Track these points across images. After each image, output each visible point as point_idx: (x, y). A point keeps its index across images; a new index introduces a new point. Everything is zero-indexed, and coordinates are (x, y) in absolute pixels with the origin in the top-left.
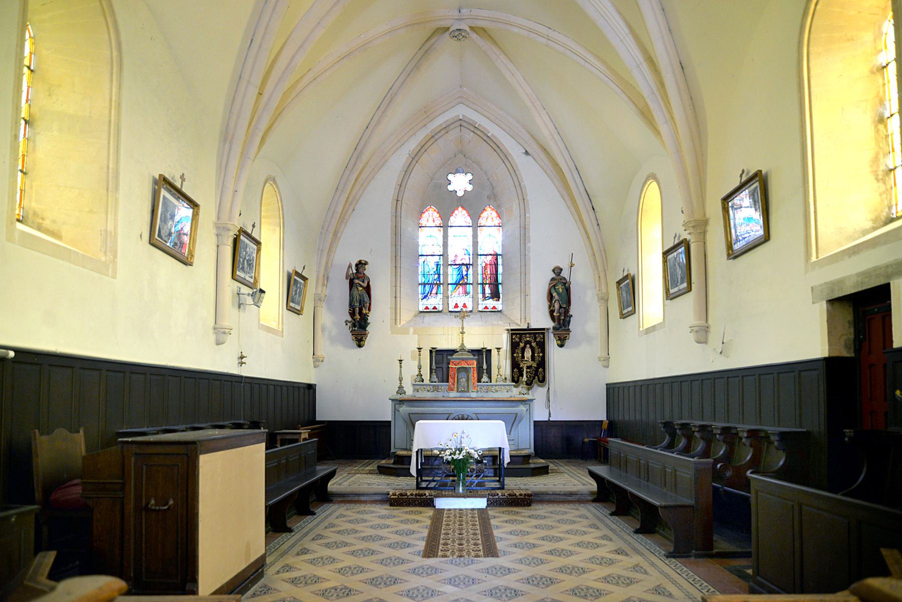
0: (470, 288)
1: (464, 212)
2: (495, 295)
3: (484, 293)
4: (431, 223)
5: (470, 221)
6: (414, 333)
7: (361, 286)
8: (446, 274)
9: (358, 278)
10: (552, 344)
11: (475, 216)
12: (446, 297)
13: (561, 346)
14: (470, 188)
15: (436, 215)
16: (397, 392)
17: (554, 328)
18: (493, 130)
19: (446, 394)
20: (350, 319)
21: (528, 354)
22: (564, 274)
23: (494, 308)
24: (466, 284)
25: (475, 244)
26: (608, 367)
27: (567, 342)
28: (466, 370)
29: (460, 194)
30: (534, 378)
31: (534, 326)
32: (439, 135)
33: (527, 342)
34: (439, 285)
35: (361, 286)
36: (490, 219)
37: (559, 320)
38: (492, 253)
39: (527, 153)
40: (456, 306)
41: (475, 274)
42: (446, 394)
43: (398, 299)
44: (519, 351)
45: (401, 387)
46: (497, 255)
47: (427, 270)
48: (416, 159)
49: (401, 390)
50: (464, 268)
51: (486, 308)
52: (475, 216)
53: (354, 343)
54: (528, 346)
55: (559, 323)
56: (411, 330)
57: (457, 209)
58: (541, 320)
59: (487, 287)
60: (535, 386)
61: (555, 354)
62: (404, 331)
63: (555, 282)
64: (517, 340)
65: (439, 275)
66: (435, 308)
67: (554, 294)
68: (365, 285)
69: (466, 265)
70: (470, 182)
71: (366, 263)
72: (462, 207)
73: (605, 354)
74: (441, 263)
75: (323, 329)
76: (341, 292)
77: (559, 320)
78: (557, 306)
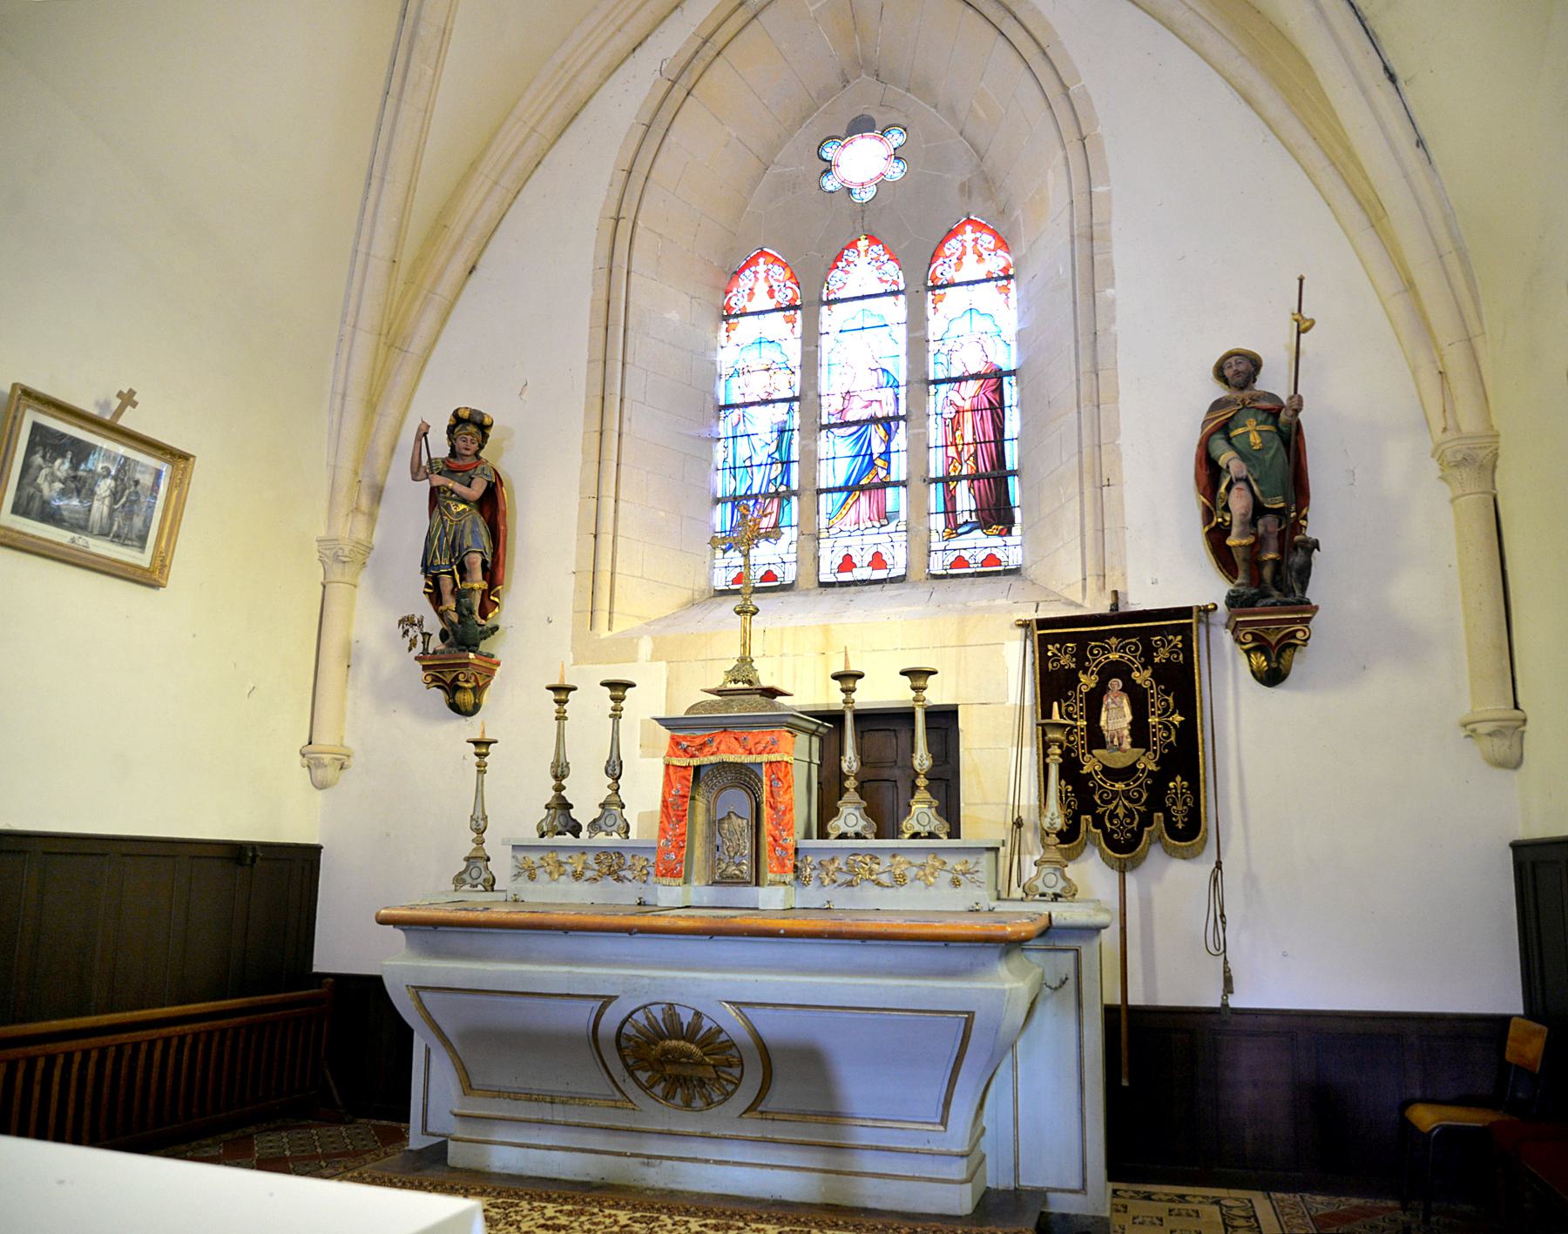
0: (895, 499)
2: (996, 514)
3: (950, 510)
4: (762, 301)
6: (655, 657)
8: (811, 460)
10: (1226, 674)
13: (1272, 677)
14: (896, 171)
17: (1233, 601)
19: (841, 899)
22: (1274, 382)
23: (991, 559)
24: (884, 485)
25: (918, 345)
26: (1517, 764)
27: (1301, 664)
30: (1147, 820)
31: (1140, 599)
33: (1110, 671)
34: (783, 497)
36: (970, 258)
37: (1255, 565)
38: (977, 366)
40: (847, 564)
41: (919, 448)
42: (841, 899)
44: (1077, 708)
45: (477, 859)
48: (685, 82)
50: (877, 434)
51: (960, 562)
54: (1116, 684)
58: (1168, 568)
59: (962, 489)
60: (1155, 856)
61: (1242, 715)
66: (769, 576)
73: (1497, 706)
74: (795, 423)
75: (350, 659)
77: (1255, 565)
78: (1239, 503)
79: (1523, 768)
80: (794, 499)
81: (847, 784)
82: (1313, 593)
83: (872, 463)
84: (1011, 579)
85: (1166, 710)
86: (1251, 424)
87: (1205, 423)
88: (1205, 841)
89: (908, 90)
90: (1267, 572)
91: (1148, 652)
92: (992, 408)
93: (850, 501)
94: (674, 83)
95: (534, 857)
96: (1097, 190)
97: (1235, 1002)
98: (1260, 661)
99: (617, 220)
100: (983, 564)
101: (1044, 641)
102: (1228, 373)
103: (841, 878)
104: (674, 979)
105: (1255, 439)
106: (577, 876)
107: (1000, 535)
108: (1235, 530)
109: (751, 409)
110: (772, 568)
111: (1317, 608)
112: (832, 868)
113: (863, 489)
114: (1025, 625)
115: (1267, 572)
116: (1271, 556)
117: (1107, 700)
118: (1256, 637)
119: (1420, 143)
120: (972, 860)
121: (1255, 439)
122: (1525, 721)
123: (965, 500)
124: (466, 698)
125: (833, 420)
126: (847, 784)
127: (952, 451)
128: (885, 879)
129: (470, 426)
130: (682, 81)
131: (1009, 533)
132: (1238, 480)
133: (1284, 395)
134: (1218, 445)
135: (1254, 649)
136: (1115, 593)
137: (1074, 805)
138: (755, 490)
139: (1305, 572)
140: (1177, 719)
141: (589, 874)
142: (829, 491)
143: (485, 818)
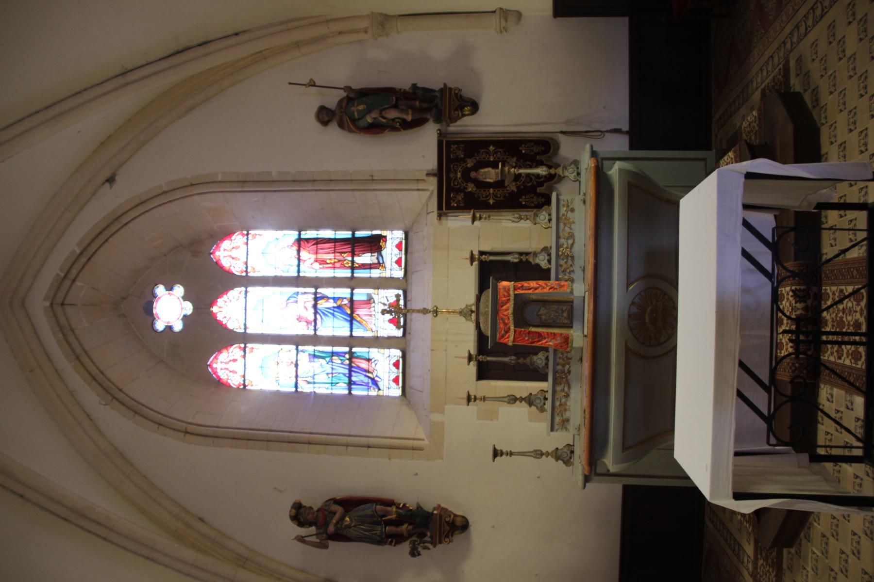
1: (220, 301)
2: (375, 244)
3: (369, 267)
5: (824, 391)
6: (441, 411)
7: (342, 518)
9: (326, 524)
11: (228, 281)
12: (378, 342)
13: (474, 107)
14: (179, 290)
15: (224, 356)
16: (568, 462)
17: (438, 120)
18: (70, 244)
20: (406, 547)
21: (490, 175)
22: (332, 100)
23: (399, 246)
24: (351, 301)
27: (467, 93)
28: (522, 304)
29: (188, 308)
31: (431, 162)
32: (75, 344)
33: (466, 177)
35: (342, 518)
36: (234, 253)
37: (422, 110)
38: (295, 248)
39: (111, 180)
43: (372, 441)
45: (557, 455)
46: (300, 242)
47: (323, 378)
49: (564, 456)
50: (323, 305)
52: (228, 281)
53: (458, 538)
54: (473, 174)
55: (429, 110)
56: (436, 417)
57: (214, 315)
58: (420, 150)
59: (359, 260)
61: (499, 114)
62: (437, 431)
63: (347, 120)
64: (460, 197)
65: (333, 354)
66: (396, 365)
67: (369, 119)
68: (339, 510)
69: (316, 299)
70: (170, 288)
71: (298, 507)
72: (212, 305)
73: (495, 20)
76: (351, 559)
77: (422, 110)
78: (392, 114)
79: (520, 10)
80: (354, 350)
81: (524, 260)
82: (436, 86)
83: (339, 307)
84: (410, 235)
85: (487, 153)
86: (354, 109)
87: (351, 131)
88: (551, 139)
89: (135, 282)
90: (425, 105)
91: (458, 160)
92: (317, 244)
93: (359, 319)
94: (114, 397)
95: (557, 419)
96: (220, 178)
97: (626, 127)
98: (467, 109)
99: (187, 432)
100: (400, 250)
101: (449, 207)
102: (326, 119)
103: (570, 262)
104: (618, 302)
105: (361, 108)
106: (567, 396)
107: (386, 241)
108: (405, 116)
109: (299, 374)
110: (392, 363)
111: (445, 85)
112: (565, 266)
113: (352, 312)
114: (440, 216)
115: (425, 105)
116: (417, 103)
117: (481, 178)
118: (456, 110)
119: (237, 34)
120: (562, 203)
121: (361, 108)
122: (501, 9)
123: (366, 258)
124: (459, 522)
125: (312, 327)
126: (524, 260)
127: (337, 265)
128: (570, 242)
129: (300, 514)
130: (112, 393)
131: (385, 237)
132: (381, 113)
133: (343, 94)
134: (362, 123)
135: (462, 111)
136: (428, 175)
137: (532, 195)
138: (347, 371)
139: (426, 90)
140: (492, 148)
141: (566, 389)
142: (351, 331)
143: (536, 451)
